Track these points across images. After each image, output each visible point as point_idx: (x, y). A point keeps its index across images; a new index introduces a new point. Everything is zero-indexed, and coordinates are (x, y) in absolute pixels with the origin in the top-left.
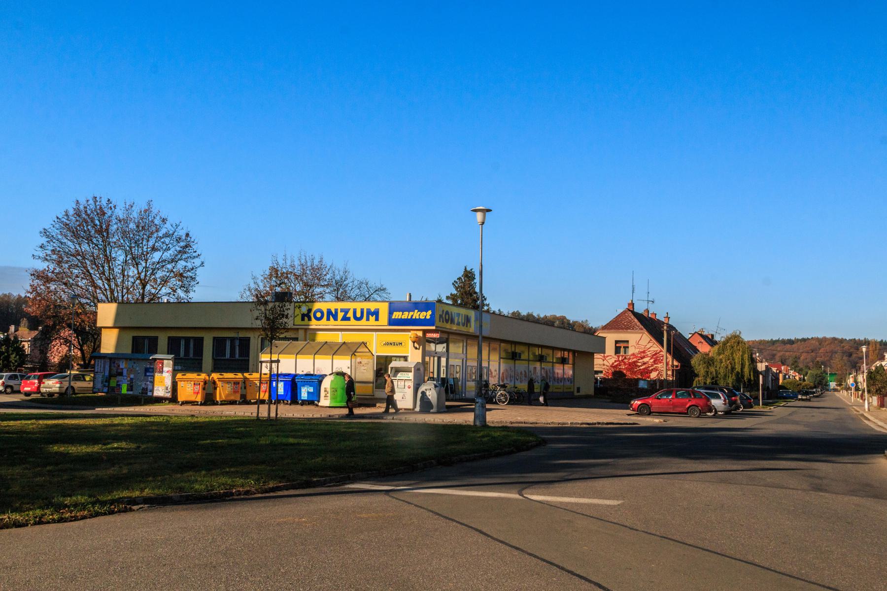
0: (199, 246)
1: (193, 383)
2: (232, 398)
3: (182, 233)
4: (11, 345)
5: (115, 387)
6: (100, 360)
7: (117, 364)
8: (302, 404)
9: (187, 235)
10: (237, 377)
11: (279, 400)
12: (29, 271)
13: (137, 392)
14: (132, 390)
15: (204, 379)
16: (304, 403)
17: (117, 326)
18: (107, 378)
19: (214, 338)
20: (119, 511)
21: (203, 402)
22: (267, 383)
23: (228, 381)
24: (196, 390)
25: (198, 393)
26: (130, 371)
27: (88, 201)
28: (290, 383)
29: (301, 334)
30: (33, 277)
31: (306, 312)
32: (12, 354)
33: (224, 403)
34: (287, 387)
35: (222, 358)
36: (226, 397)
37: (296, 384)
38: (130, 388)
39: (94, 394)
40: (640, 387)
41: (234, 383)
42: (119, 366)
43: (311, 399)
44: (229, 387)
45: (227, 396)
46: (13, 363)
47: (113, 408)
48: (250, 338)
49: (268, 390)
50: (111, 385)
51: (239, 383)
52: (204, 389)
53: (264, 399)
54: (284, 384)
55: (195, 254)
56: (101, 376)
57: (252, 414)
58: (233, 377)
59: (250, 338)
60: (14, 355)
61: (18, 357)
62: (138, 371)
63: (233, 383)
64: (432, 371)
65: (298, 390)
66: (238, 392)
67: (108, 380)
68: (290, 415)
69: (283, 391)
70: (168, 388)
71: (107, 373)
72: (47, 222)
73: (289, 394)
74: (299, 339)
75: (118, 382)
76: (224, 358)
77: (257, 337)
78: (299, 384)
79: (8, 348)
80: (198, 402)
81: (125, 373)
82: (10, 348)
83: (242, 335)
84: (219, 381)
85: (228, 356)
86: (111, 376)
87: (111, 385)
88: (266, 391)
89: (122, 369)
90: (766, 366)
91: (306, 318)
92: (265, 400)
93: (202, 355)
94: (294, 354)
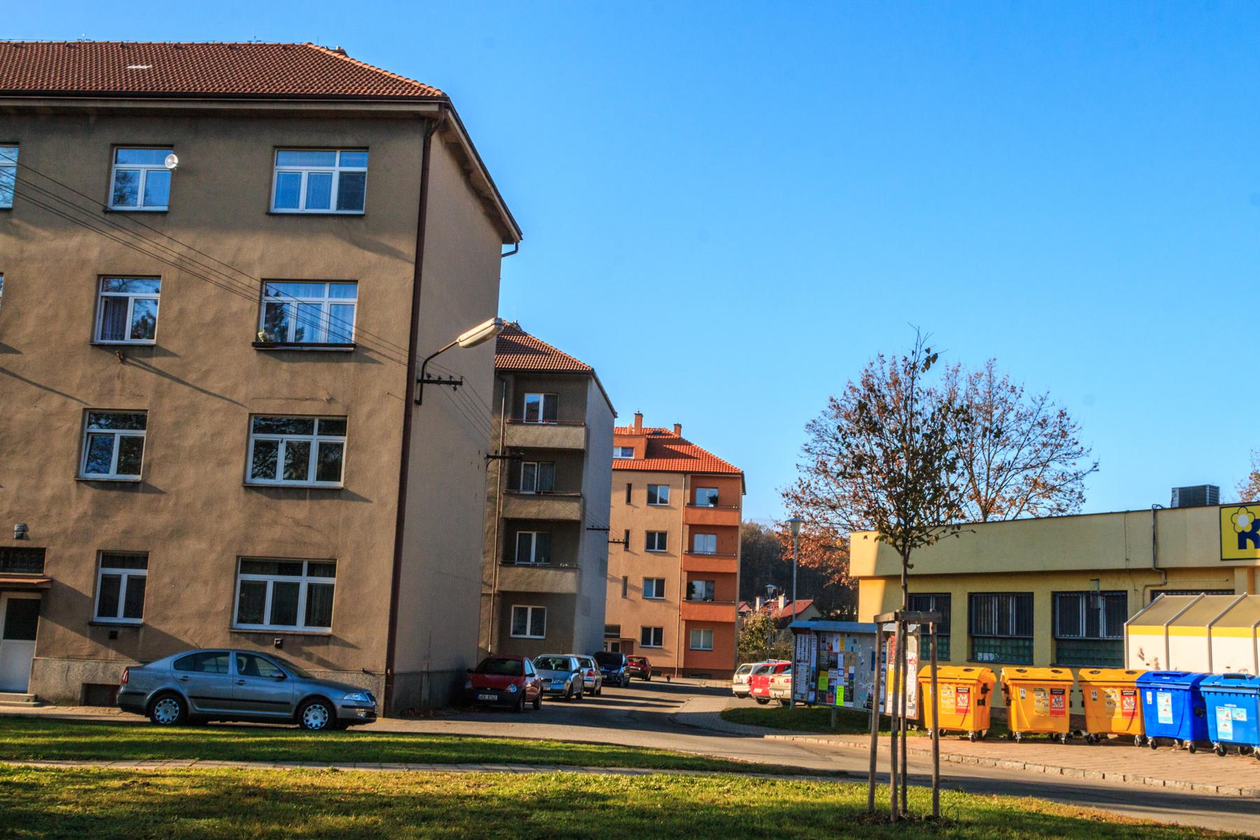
0: (1083, 436)
1: (953, 687)
2: (1049, 726)
3: (1052, 413)
5: (826, 692)
6: (803, 636)
7: (828, 644)
8: (1222, 752)
9: (1062, 414)
10: (1059, 676)
11: (1162, 740)
12: (779, 489)
13: (858, 705)
14: (851, 700)
15: (979, 681)
16: (1227, 749)
17: (878, 574)
18: (813, 672)
19: (1054, 594)
21: (984, 732)
22: (1135, 694)
23: (1035, 686)
24: (962, 705)
25: (966, 711)
26: (850, 659)
27: (871, 364)
28: (1187, 695)
29: (1241, 578)
30: (786, 499)
31: (1248, 529)
33: (1029, 738)
34: (1181, 705)
35: (1072, 637)
36: (1032, 726)
37: (1203, 700)
38: (849, 696)
39: (41, 705)
41: (1052, 692)
42: (831, 648)
43: (1241, 740)
44: (1039, 701)
45: (1039, 719)
47: (792, 737)
48: (1126, 591)
49: (1138, 710)
50: (820, 688)
51: (1063, 692)
52: (981, 703)
53: (1128, 732)
54: (1173, 698)
55: (1076, 448)
56: (805, 669)
57: (1062, 772)
58: (1050, 678)
59: (1126, 591)
62: (860, 658)
63: (1048, 691)
64: (418, 399)
65: (1209, 716)
66: (1063, 713)
67: (815, 679)
68: (1155, 782)
69: (1170, 714)
70: (912, 699)
71: (814, 665)
72: (817, 408)
73: (1187, 723)
74: (1236, 591)
75: (830, 680)
76: (1076, 637)
77: (1140, 589)
78: (1208, 699)
80: (967, 732)
81: (840, 664)
83: (1107, 585)
84: (1013, 685)
85: (1083, 633)
86: (820, 669)
87: (820, 688)
88: (1133, 714)
89: (836, 654)
91: (1249, 542)
92: (1134, 736)
93: (1031, 632)
94: (1202, 625)
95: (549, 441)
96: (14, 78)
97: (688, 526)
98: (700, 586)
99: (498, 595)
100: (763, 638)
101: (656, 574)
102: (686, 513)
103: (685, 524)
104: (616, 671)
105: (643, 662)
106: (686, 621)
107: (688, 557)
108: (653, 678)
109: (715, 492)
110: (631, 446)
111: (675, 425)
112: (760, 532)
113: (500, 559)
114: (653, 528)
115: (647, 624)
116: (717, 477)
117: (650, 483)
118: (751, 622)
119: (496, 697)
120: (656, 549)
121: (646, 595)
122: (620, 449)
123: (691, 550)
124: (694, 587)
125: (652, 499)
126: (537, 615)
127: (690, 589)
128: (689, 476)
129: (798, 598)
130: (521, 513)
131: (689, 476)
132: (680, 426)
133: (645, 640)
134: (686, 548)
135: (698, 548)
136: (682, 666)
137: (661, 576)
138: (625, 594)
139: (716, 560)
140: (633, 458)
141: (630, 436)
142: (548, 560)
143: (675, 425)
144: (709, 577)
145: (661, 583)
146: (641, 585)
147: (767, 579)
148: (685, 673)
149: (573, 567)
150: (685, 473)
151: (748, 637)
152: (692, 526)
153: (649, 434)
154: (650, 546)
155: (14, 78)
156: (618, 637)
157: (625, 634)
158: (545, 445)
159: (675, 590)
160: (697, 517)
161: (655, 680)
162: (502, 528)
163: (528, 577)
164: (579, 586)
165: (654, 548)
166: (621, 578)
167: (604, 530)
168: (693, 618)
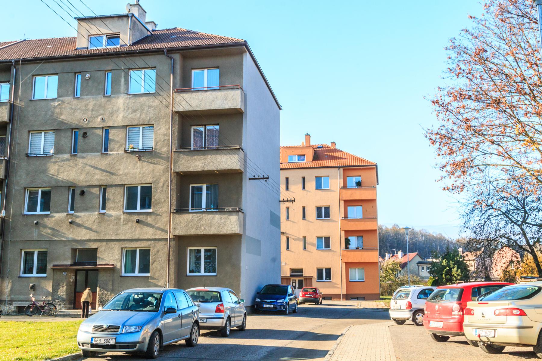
4: (451, 258)
20: (14, 315)
32: (453, 268)
40: (185, 343)
46: (455, 277)
60: (455, 269)
61: (459, 270)
79: (449, 262)
82: (451, 262)
90: (103, 326)
95: (211, 104)
96: (51, 52)
97: (343, 202)
98: (353, 240)
99: (174, 239)
100: (393, 274)
101: (324, 234)
102: (340, 193)
103: (341, 200)
104: (281, 301)
105: (315, 291)
106: (346, 263)
107: (344, 221)
108: (324, 302)
109: (360, 179)
110: (304, 154)
111: (332, 143)
112: (382, 228)
113: (174, 208)
114: (320, 204)
115: (320, 267)
116: (360, 169)
117: (317, 175)
118: (386, 265)
119: (272, 306)
120: (323, 218)
121: (319, 247)
122: (297, 156)
123: (346, 217)
124: (349, 241)
125: (318, 186)
126: (210, 257)
127: (347, 242)
128: (341, 169)
129: (410, 252)
130: (189, 167)
131: (341, 169)
132: (334, 143)
133: (320, 277)
134: (342, 215)
135: (350, 215)
136: (345, 292)
137: (327, 235)
138: (305, 248)
139: (363, 223)
140: (305, 161)
141: (303, 148)
142: (216, 206)
143: (332, 143)
144: (359, 233)
145: (328, 240)
146: (315, 241)
147: (387, 250)
148: (348, 297)
149: (238, 211)
150: (339, 167)
151: (384, 274)
152: (345, 201)
153: (315, 148)
154: (319, 215)
155: (51, 52)
156: (302, 276)
157: (306, 274)
158: (208, 108)
159: (337, 243)
160: (349, 195)
161: (326, 304)
162: (175, 181)
163: (198, 222)
164: (244, 225)
165: (322, 217)
166: (302, 238)
167: (264, 178)
168: (350, 261)
